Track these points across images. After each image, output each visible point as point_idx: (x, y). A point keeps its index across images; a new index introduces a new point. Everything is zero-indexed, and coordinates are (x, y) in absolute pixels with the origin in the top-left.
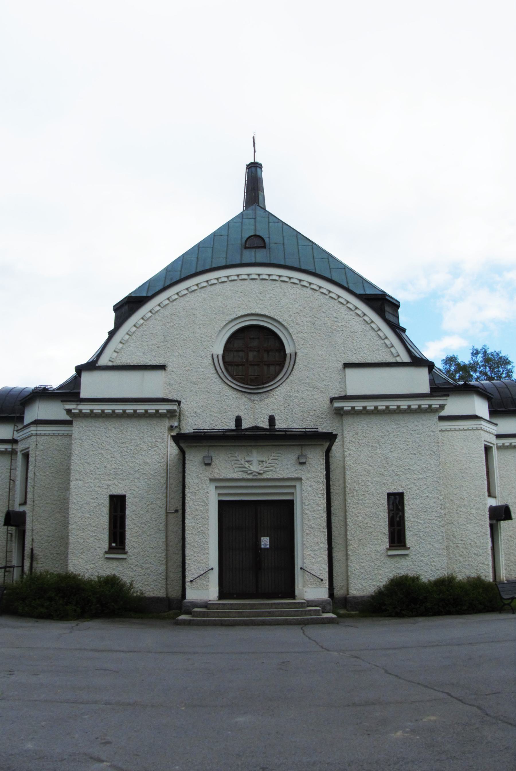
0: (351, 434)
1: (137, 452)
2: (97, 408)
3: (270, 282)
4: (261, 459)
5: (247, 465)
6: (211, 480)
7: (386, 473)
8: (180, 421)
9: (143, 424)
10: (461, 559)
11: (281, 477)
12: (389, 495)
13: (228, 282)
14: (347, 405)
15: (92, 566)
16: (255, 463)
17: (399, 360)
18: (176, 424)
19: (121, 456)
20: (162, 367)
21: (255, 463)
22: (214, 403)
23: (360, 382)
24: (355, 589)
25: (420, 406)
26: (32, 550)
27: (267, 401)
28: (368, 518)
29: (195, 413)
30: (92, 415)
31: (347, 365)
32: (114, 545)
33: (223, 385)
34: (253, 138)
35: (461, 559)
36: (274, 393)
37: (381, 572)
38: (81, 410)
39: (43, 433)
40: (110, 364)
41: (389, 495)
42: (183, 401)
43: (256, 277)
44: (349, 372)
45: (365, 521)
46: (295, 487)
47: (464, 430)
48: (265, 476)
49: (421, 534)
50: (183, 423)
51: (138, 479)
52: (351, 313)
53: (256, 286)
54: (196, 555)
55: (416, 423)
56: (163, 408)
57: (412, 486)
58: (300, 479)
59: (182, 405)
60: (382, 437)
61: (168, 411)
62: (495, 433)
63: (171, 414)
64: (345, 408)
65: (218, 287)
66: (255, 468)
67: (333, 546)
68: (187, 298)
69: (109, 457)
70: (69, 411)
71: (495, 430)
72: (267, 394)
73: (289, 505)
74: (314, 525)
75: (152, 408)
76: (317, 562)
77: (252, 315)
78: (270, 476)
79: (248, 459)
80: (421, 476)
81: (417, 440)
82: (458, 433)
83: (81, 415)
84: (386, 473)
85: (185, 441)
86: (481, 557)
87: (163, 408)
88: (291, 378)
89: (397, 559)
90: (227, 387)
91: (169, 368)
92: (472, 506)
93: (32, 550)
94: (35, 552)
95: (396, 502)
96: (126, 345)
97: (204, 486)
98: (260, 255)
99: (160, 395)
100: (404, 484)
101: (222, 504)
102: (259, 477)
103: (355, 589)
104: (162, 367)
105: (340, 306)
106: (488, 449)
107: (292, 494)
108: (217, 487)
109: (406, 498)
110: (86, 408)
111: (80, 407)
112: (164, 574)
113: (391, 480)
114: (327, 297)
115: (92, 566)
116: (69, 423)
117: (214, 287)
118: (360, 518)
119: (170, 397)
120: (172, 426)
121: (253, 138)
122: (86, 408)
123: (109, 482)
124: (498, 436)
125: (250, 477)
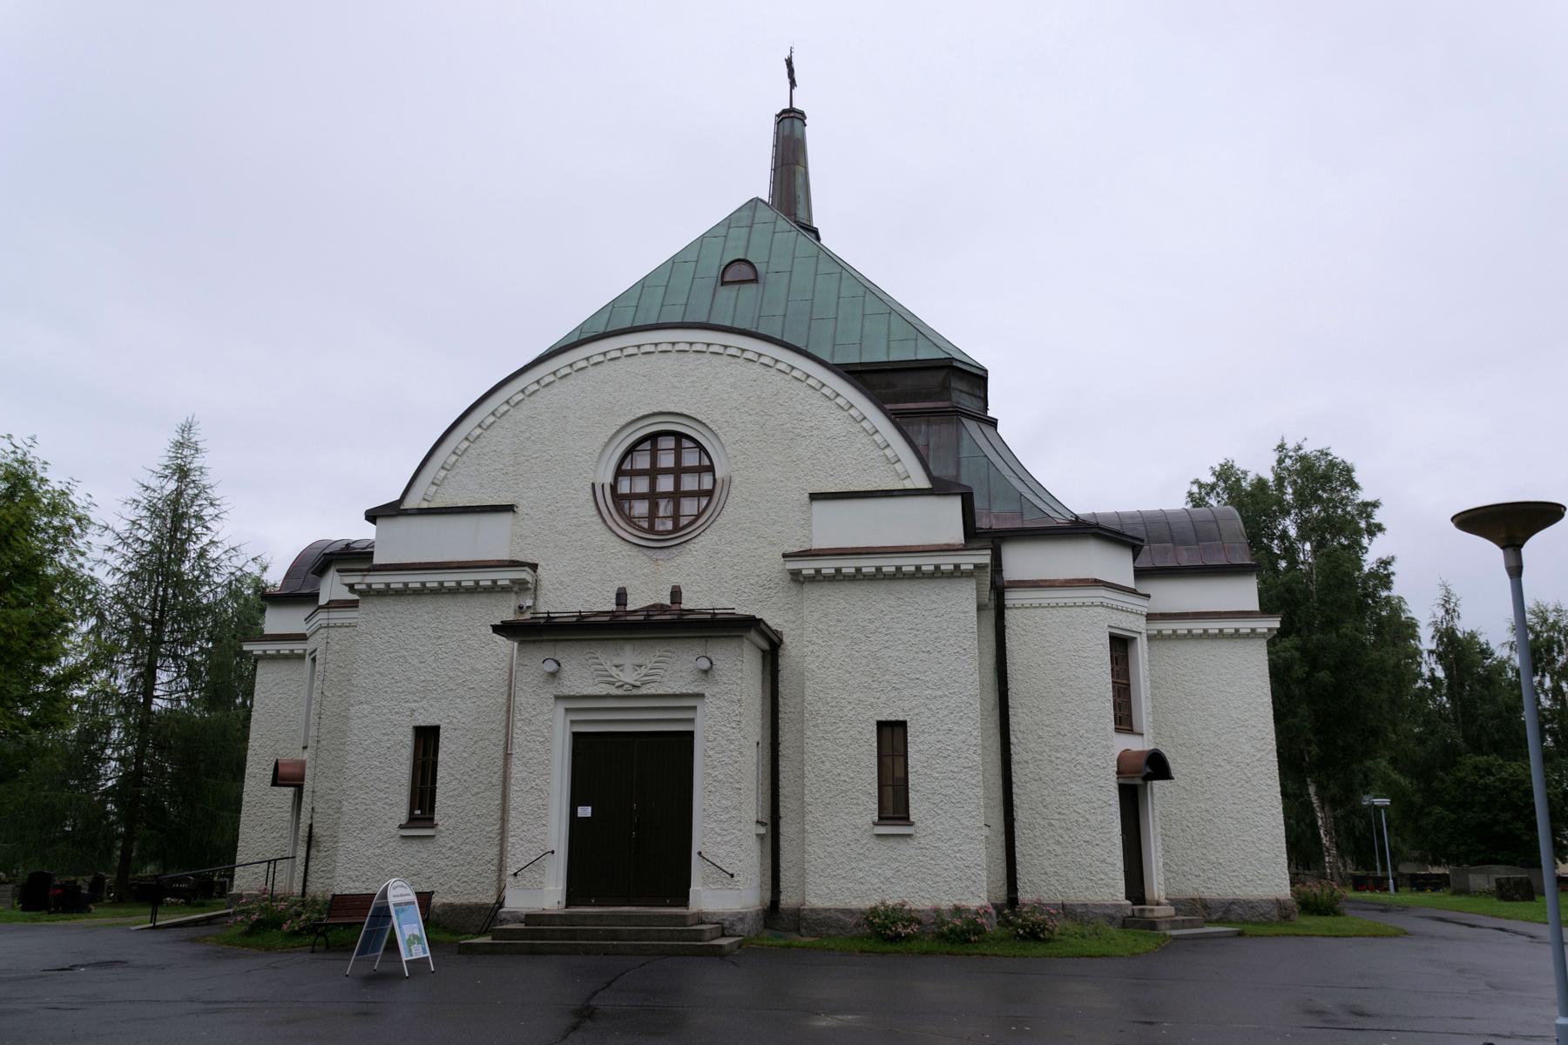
0: (816, 616)
1: (15, 602)
2: (397, 581)
3: (693, 355)
4: (639, 660)
5: (614, 671)
6: (557, 698)
7: (875, 685)
8: (535, 598)
9: (446, 603)
10: (1059, 850)
11: (671, 691)
12: (881, 725)
13: (707, 355)
14: (808, 567)
15: (378, 851)
16: (628, 667)
17: (908, 485)
18: (529, 603)
19: (435, 661)
20: (509, 508)
21: (628, 667)
22: (589, 568)
23: (840, 527)
24: (816, 895)
25: (937, 567)
26: (311, 826)
27: (679, 560)
28: (838, 769)
29: (561, 583)
30: (387, 593)
31: (814, 497)
32: (418, 812)
33: (609, 534)
34: (793, 84)
35: (1059, 850)
36: (690, 546)
37: (862, 865)
38: (369, 585)
39: (339, 622)
40: (425, 505)
41: (881, 725)
42: (541, 563)
43: (618, 354)
44: (818, 506)
45: (836, 771)
46: (694, 708)
47: (1066, 605)
48: (644, 691)
49: (937, 799)
50: (541, 600)
51: (462, 697)
52: (829, 403)
53: (670, 362)
54: (525, 828)
55: (934, 597)
56: (504, 577)
57: (923, 709)
58: (702, 696)
59: (539, 570)
60: (871, 622)
61: (514, 581)
62: (1145, 611)
63: (520, 587)
64: (812, 571)
65: (607, 368)
66: (629, 677)
67: (782, 813)
68: (554, 389)
69: (416, 662)
70: (351, 587)
71: (1144, 606)
72: (680, 548)
73: (682, 743)
74: (721, 777)
75: (485, 578)
76: (726, 843)
77: (655, 414)
78: (653, 691)
79: (617, 661)
80: (939, 693)
81: (935, 628)
82: (1054, 611)
83: (368, 593)
84: (875, 685)
85: (530, 631)
86: (1098, 849)
87: (504, 577)
88: (720, 520)
89: (891, 842)
90: (614, 538)
91: (521, 510)
92: (1080, 749)
93: (311, 826)
94: (315, 830)
95: (892, 734)
96: (453, 473)
97: (545, 709)
98: (736, 303)
99: (504, 556)
100: (907, 705)
101: (577, 737)
102: (635, 692)
103: (816, 895)
104: (509, 508)
105: (811, 392)
106: (1120, 645)
107: (692, 721)
108: (567, 710)
109: (910, 731)
110: (378, 581)
111: (368, 580)
112: (496, 861)
113: (884, 698)
114: (788, 378)
115: (378, 851)
116: (352, 604)
117: (599, 368)
118: (828, 765)
119: (521, 558)
120: (521, 608)
121: (793, 84)
122: (378, 581)
123: (414, 705)
124: (1151, 617)
125: (620, 692)
